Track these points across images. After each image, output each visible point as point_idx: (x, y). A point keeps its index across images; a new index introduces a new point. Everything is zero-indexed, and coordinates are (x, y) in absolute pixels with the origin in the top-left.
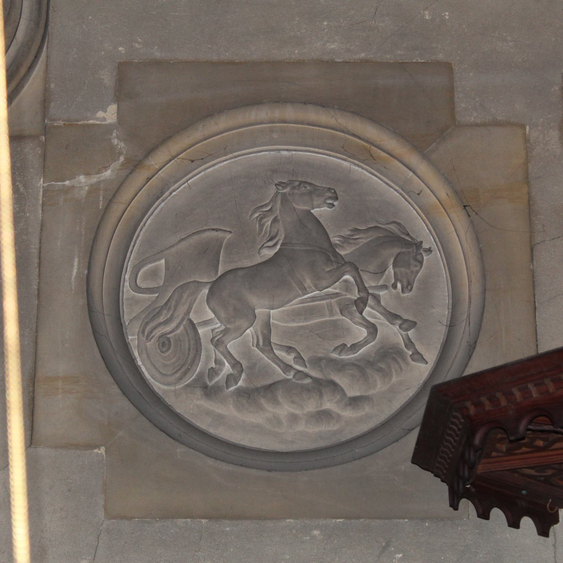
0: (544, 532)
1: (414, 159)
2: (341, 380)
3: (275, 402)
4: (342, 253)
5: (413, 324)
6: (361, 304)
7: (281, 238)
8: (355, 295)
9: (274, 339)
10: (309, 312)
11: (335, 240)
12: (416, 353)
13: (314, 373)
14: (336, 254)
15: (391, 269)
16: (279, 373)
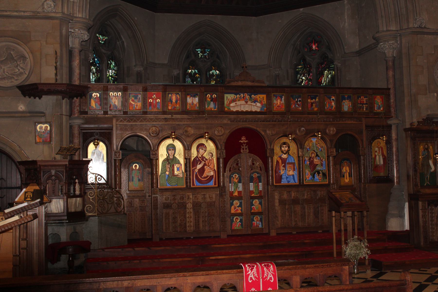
0: (40, 99)
1: (25, 46)
2: (15, 77)
3: (5, 80)
4: (15, 58)
5: (25, 69)
6: (17, 66)
7: (6, 56)
8: (16, 65)
9: (5, 71)
10: (10, 67)
11: (14, 56)
12: (25, 73)
13: (11, 76)
14: (14, 59)
15: (22, 61)
16: (5, 76)
